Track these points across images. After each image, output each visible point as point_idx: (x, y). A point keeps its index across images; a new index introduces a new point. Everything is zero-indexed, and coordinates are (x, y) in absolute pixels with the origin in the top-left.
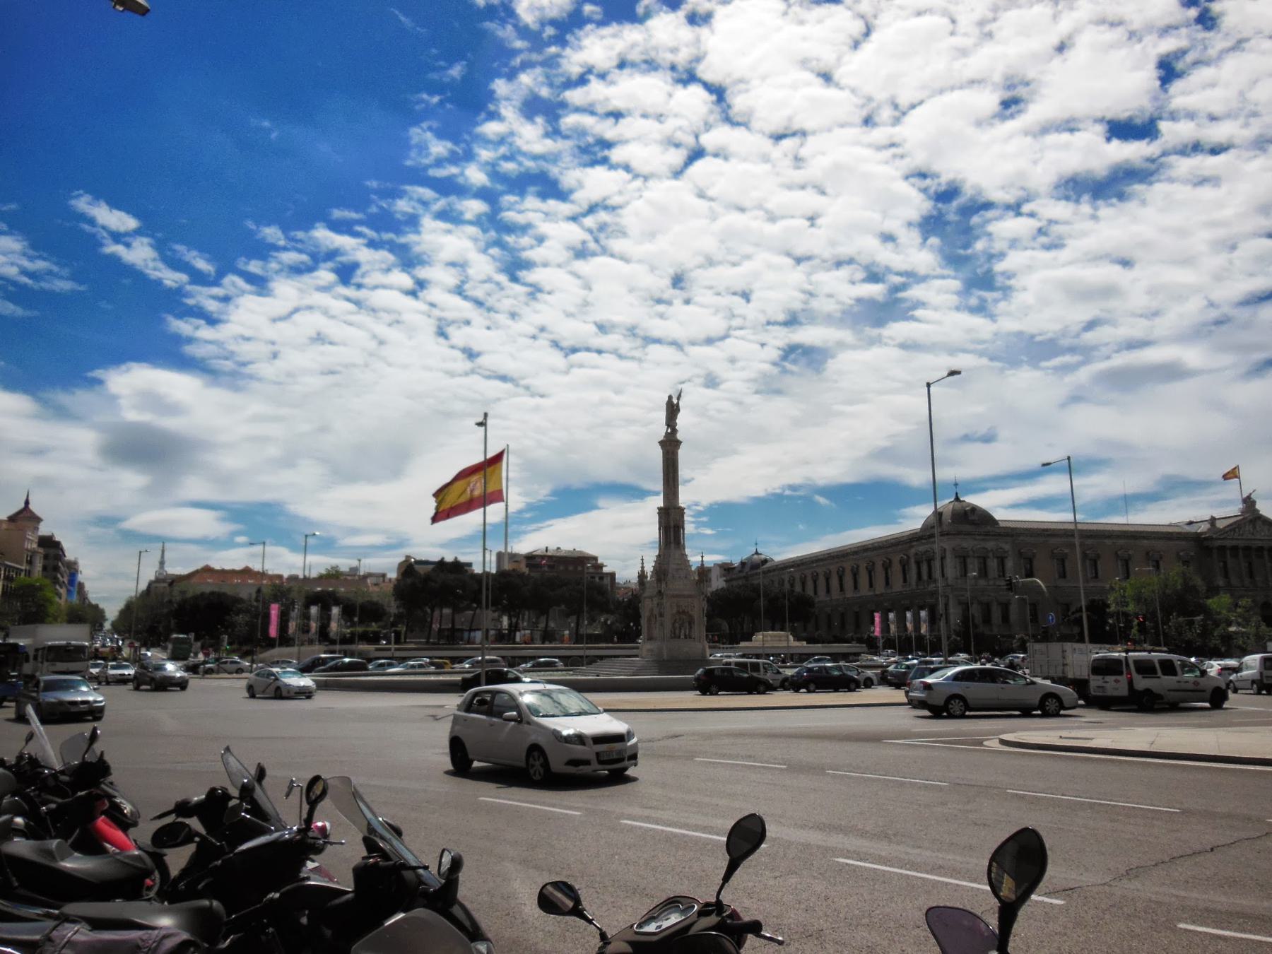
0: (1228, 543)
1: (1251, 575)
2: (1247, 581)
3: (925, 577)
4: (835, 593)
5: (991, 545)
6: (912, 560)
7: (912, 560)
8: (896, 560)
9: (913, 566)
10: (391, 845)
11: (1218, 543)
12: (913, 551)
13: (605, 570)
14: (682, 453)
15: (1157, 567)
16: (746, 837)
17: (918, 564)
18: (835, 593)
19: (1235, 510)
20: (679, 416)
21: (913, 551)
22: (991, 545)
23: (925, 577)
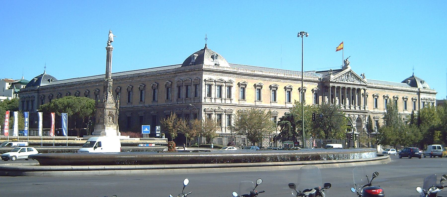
12: (176, 79)
17: (179, 88)
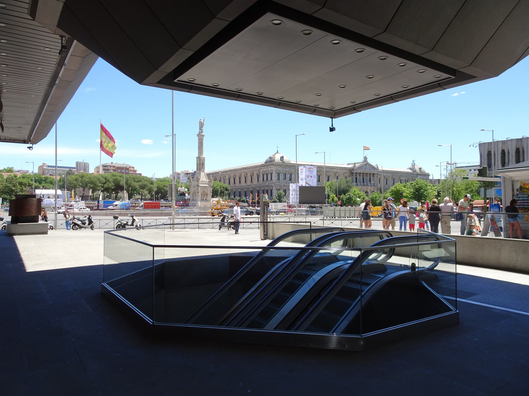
0: (359, 171)
1: (370, 181)
2: (362, 184)
3: (265, 179)
4: (249, 182)
5: (287, 170)
6: (261, 174)
7: (261, 174)
8: (255, 173)
9: (262, 176)
10: (195, 214)
11: (356, 171)
12: (262, 170)
13: (137, 172)
14: (205, 139)
15: (338, 178)
16: (332, 129)
18: (249, 182)
19: (361, 160)
20: (204, 126)
21: (262, 170)
22: (287, 170)
23: (265, 179)
